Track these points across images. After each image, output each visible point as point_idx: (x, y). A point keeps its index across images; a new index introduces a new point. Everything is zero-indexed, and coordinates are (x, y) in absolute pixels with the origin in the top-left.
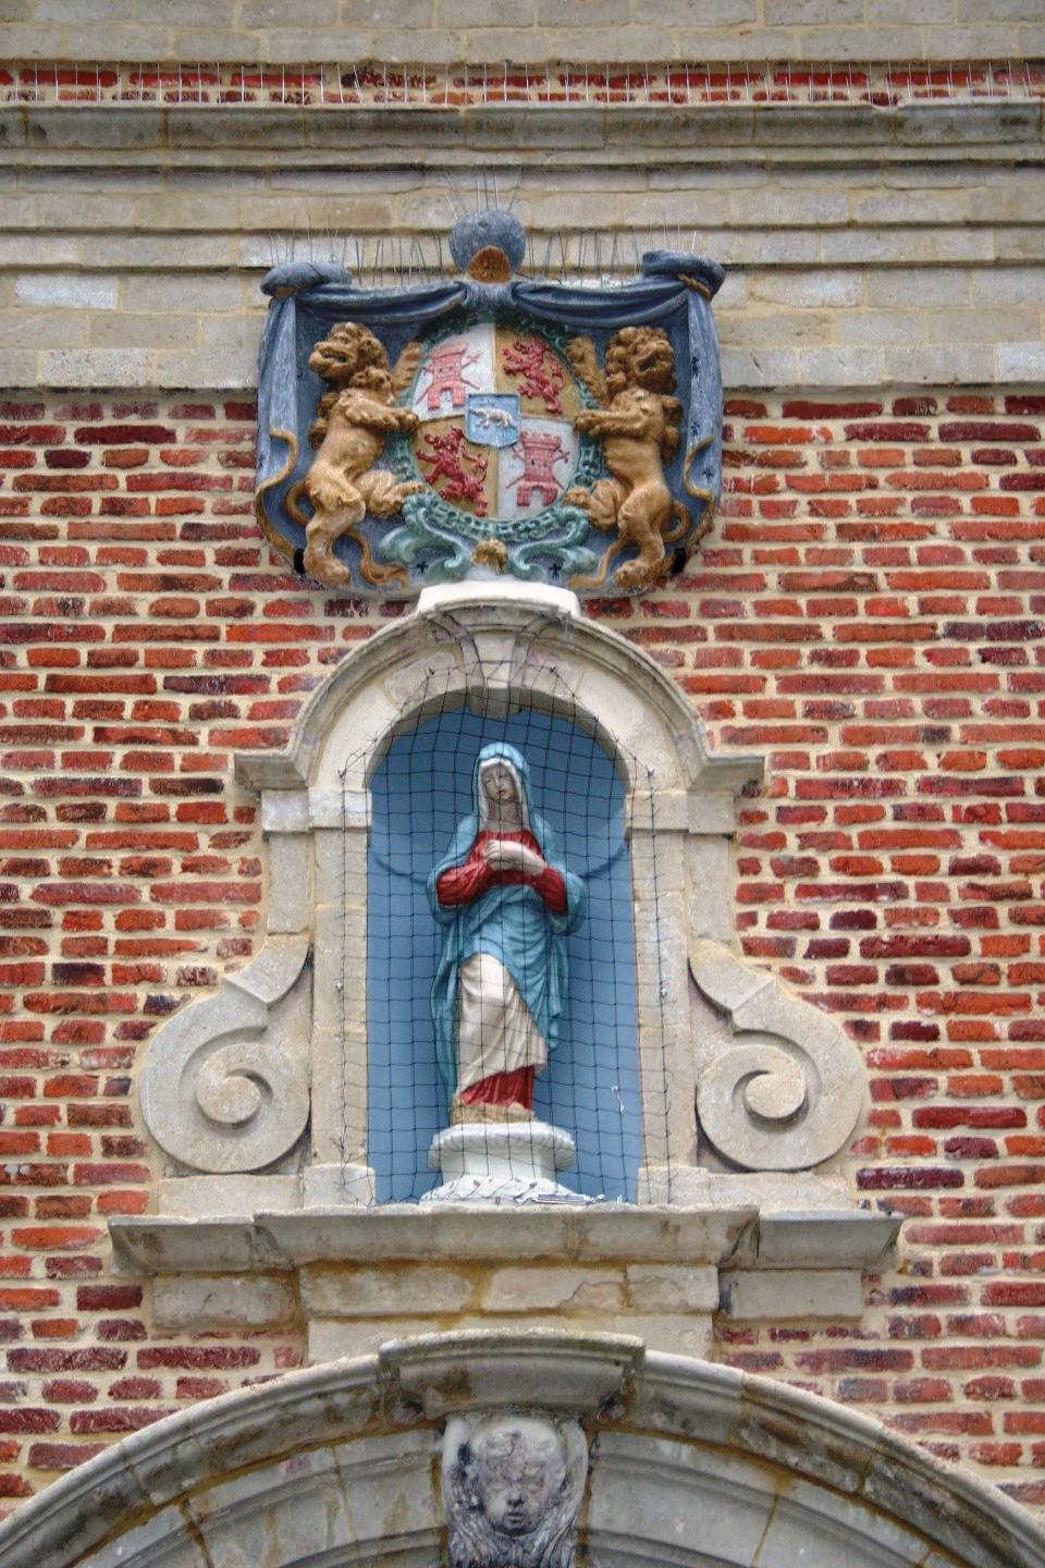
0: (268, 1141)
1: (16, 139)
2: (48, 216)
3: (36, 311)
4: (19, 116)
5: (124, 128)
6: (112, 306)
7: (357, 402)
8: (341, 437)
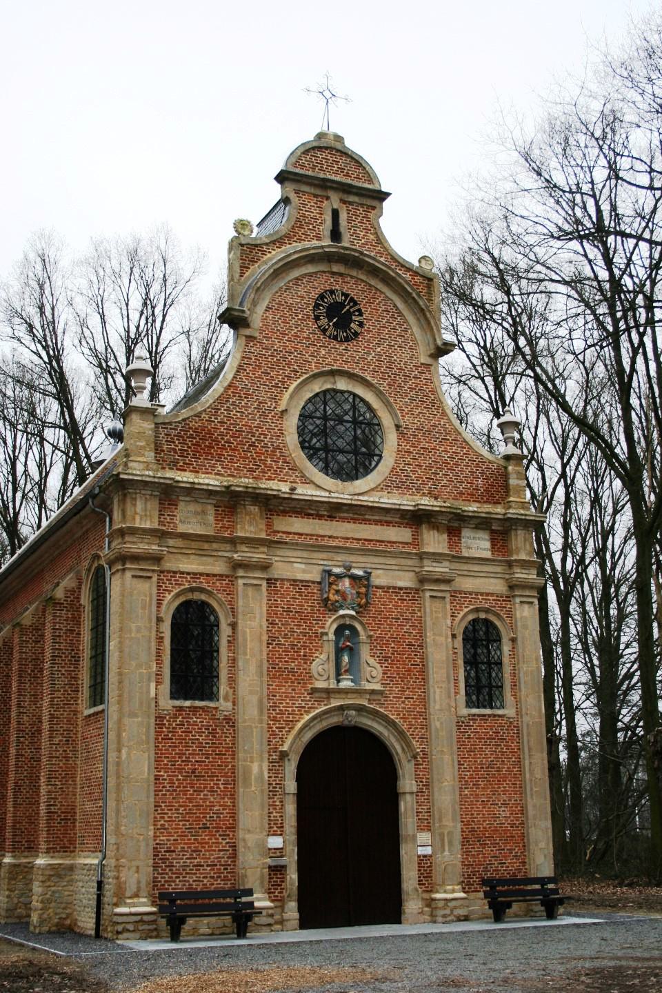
0: (325, 677)
7: (334, 587)
8: (332, 591)
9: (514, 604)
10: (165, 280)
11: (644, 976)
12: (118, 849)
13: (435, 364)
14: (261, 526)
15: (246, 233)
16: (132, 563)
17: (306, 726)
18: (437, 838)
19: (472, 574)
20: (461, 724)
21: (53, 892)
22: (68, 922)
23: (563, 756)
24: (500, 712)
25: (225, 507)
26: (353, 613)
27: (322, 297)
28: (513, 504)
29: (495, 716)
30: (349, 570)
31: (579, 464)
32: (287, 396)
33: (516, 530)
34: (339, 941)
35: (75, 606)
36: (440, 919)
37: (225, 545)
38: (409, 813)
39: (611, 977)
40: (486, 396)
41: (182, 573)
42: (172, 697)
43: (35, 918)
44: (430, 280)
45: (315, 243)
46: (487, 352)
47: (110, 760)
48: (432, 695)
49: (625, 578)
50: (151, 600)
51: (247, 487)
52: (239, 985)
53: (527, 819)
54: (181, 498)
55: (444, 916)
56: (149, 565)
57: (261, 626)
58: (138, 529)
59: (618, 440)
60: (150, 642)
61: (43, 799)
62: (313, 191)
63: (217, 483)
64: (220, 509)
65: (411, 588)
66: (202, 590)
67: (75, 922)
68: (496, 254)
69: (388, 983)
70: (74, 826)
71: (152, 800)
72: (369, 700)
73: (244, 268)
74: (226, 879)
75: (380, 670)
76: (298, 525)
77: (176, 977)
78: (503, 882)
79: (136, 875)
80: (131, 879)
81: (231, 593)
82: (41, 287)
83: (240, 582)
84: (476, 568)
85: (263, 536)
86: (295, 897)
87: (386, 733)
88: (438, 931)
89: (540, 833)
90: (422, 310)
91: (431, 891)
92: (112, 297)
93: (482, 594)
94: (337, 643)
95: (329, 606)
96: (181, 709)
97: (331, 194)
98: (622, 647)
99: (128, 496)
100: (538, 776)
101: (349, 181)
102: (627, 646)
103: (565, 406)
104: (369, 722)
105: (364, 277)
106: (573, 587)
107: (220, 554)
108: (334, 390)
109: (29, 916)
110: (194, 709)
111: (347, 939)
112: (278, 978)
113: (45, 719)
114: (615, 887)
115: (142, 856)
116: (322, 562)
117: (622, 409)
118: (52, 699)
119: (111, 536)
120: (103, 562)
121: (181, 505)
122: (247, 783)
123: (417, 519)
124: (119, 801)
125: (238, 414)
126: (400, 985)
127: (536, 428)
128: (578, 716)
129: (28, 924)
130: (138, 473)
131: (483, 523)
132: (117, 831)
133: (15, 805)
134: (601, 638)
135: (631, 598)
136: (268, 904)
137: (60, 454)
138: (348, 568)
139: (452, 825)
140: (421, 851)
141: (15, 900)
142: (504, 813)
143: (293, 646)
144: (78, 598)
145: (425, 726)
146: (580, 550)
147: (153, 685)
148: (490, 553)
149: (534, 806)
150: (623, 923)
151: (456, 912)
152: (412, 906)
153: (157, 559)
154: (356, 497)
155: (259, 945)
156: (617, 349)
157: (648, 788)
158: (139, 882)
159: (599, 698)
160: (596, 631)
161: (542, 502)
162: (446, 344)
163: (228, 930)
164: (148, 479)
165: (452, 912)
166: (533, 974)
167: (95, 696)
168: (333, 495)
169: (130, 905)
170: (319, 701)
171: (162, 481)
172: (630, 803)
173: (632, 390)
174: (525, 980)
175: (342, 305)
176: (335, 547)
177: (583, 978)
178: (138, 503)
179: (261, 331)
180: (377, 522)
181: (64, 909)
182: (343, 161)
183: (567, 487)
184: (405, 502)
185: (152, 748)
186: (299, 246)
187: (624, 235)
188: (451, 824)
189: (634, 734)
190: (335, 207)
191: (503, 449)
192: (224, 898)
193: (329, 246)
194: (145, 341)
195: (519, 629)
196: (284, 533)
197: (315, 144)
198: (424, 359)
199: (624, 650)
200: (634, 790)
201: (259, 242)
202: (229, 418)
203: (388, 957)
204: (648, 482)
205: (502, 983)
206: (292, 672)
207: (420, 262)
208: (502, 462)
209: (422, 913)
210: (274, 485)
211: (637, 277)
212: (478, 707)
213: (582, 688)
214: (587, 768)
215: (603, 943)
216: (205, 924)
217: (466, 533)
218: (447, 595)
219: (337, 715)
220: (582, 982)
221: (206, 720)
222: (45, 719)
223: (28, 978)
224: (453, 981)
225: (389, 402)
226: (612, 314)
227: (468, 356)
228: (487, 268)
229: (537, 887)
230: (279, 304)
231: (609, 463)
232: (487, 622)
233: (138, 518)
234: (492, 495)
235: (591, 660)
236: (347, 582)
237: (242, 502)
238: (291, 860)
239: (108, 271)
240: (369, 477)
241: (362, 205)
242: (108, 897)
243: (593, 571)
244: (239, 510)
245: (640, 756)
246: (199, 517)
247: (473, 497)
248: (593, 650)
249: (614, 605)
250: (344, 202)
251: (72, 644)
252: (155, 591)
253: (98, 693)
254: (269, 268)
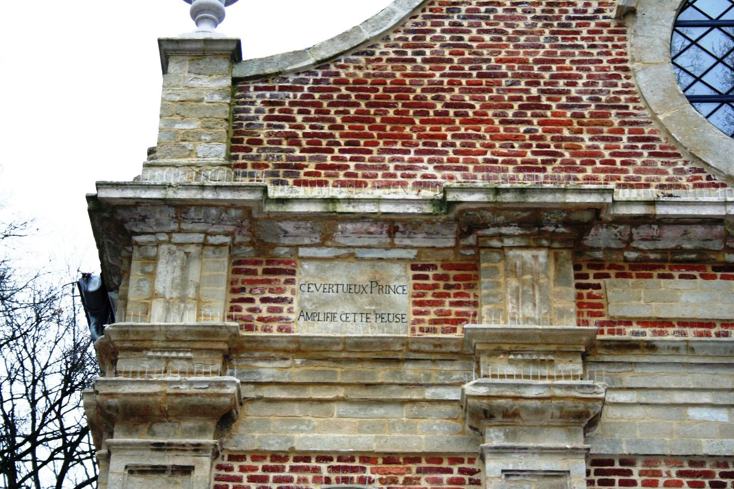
1: (683, 352)
2: (698, 383)
3: (697, 422)
4: (685, 343)
5: (726, 348)
6: (726, 421)
14: (558, 305)
16: (129, 432)
25: (448, 266)
37: (447, 367)
56: (188, 432)
64: (430, 273)
107: (429, 394)
121: (306, 272)
125: (487, 37)
164: (183, 195)
219: (504, 203)
237: (495, 243)
246: (363, 300)
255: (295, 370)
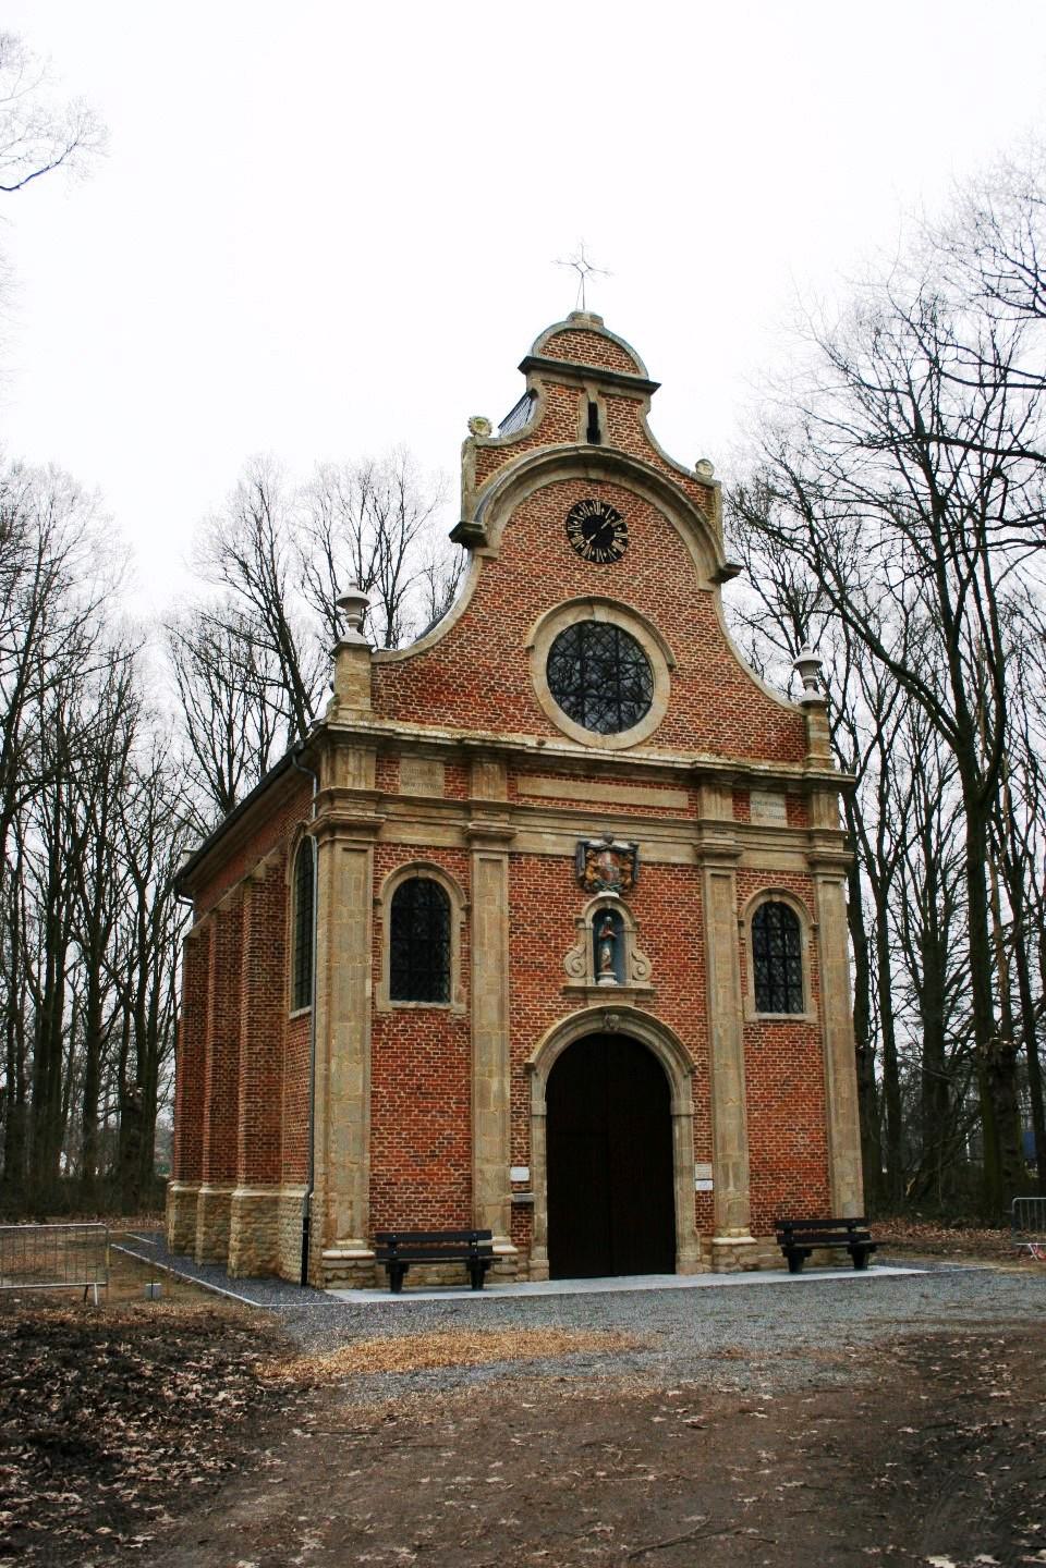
0: (581, 974)
7: (592, 863)
8: (590, 869)
9: (816, 885)
10: (402, 508)
11: (974, 1347)
12: (327, 1181)
13: (716, 590)
15: (483, 432)
16: (342, 834)
17: (558, 1033)
18: (720, 1173)
19: (763, 847)
20: (750, 1031)
21: (255, 1230)
22: (272, 1265)
23: (879, 1073)
24: (798, 1017)
26: (616, 895)
27: (576, 509)
28: (813, 762)
29: (791, 1021)
30: (610, 843)
31: (898, 725)
32: (533, 629)
33: (818, 793)
34: (596, 1295)
35: (277, 887)
36: (722, 1268)
38: (685, 1140)
39: (932, 1346)
40: (786, 645)
41: (405, 845)
42: (393, 998)
43: (233, 1260)
44: (710, 488)
45: (569, 445)
46: (786, 589)
47: (317, 1072)
48: (713, 996)
49: (952, 862)
50: (366, 878)
51: (484, 741)
52: (458, 1353)
53: (831, 1147)
54: (403, 754)
55: (728, 1265)
57: (502, 912)
58: (351, 791)
59: (945, 698)
60: (365, 929)
61: (242, 1119)
62: (564, 381)
63: (448, 736)
65: (688, 865)
66: (429, 867)
67: (280, 1266)
68: (794, 469)
69: (645, 1354)
70: (279, 1152)
71: (368, 1121)
72: (636, 1002)
73: (480, 475)
74: (458, 1218)
75: (650, 965)
76: (548, 787)
77: (384, 1339)
78: (801, 1224)
79: (349, 1212)
80: (343, 1216)
81: (466, 870)
82: (259, 522)
83: (476, 856)
84: (768, 840)
85: (504, 800)
86: (545, 1241)
87: (656, 1042)
88: (719, 1284)
89: (847, 1164)
90: (700, 524)
91: (712, 1235)
92: (341, 531)
93: (776, 872)
94: (595, 932)
95: (587, 887)
96: (403, 1011)
97: (586, 385)
98: (950, 944)
99: (339, 752)
100: (845, 1095)
101: (610, 370)
102: (957, 942)
103: (877, 650)
104: (635, 1029)
105: (628, 486)
106: (892, 871)
107: (451, 822)
108: (592, 622)
109: (227, 1257)
110: (420, 1012)
111: (603, 1293)
112: (509, 1344)
113: (244, 1022)
114: (940, 1229)
115: (356, 1189)
116: (577, 833)
117: (949, 658)
118: (251, 1000)
119: (319, 801)
120: (309, 833)
121: (404, 762)
122: (484, 1103)
123: (694, 780)
124: (327, 1122)
126: (660, 1356)
127: (846, 680)
128: (897, 1024)
129: (226, 1265)
130: (350, 723)
131: (775, 785)
132: (326, 1160)
133: (213, 1126)
134: (924, 932)
135: (961, 886)
136: (511, 1249)
137: (283, 717)
138: (610, 840)
139: (737, 1155)
140: (700, 1186)
141: (214, 1238)
142: (802, 1140)
143: (541, 935)
144: (283, 878)
145: (707, 1034)
146: (899, 828)
147: (369, 982)
148: (785, 822)
149: (840, 1132)
150: (948, 1275)
151: (743, 1260)
152: (688, 1252)
153: (373, 828)
154: (619, 753)
155: (497, 1299)
156: (942, 584)
157: (980, 1110)
158: (352, 1220)
159: (922, 1005)
160: (920, 925)
161: (857, 768)
162: (730, 566)
163: (461, 1279)
164: (362, 731)
165: (738, 1260)
166: (833, 1343)
167: (302, 995)
168: (590, 750)
169: (342, 1248)
170: (574, 1002)
171: (379, 733)
172: (960, 1128)
173: (961, 636)
174: (821, 1351)
175: (602, 519)
176: (594, 814)
177: (896, 1349)
178: (351, 760)
179: (501, 551)
180: (645, 784)
181: (268, 1249)
182: (601, 345)
183: (883, 753)
184: (680, 759)
185: (369, 1060)
186: (548, 448)
187: (948, 441)
188: (737, 1154)
189: (964, 1047)
190: (593, 400)
191: (801, 693)
192: (458, 1241)
193: (584, 447)
194: (380, 583)
195: (822, 915)
196: (529, 796)
197: (567, 326)
198: (703, 584)
199: (952, 948)
200: (964, 1114)
201: (498, 444)
202: (462, 656)
203: (654, 1317)
204: (981, 747)
205: (791, 1356)
206: (540, 967)
207: (697, 466)
208: (800, 710)
209: (701, 1261)
210: (517, 738)
211: (966, 497)
212: (771, 1011)
213: (902, 992)
214: (908, 1088)
215: (924, 1300)
216: (433, 1272)
217: (756, 797)
218: (733, 873)
220: (896, 1354)
221: (434, 1024)
222: (244, 1022)
223: (206, 1335)
224: (729, 1352)
225: (658, 636)
226: (936, 539)
227: (763, 596)
228: (784, 486)
229: (843, 1230)
230: (524, 517)
231: (935, 721)
232: (783, 907)
233: (350, 779)
234: (788, 751)
235: (913, 960)
236: (608, 857)
238: (539, 1196)
239: (336, 501)
240: (636, 728)
241: (626, 398)
242: (317, 1237)
243: (915, 853)
244: (475, 769)
245: (971, 1073)
246: (426, 778)
247: (763, 752)
248: (915, 948)
249: (940, 893)
250: (604, 395)
251: (274, 933)
252: (371, 867)
253: (304, 995)
254: (511, 475)
255: (401, 809)
